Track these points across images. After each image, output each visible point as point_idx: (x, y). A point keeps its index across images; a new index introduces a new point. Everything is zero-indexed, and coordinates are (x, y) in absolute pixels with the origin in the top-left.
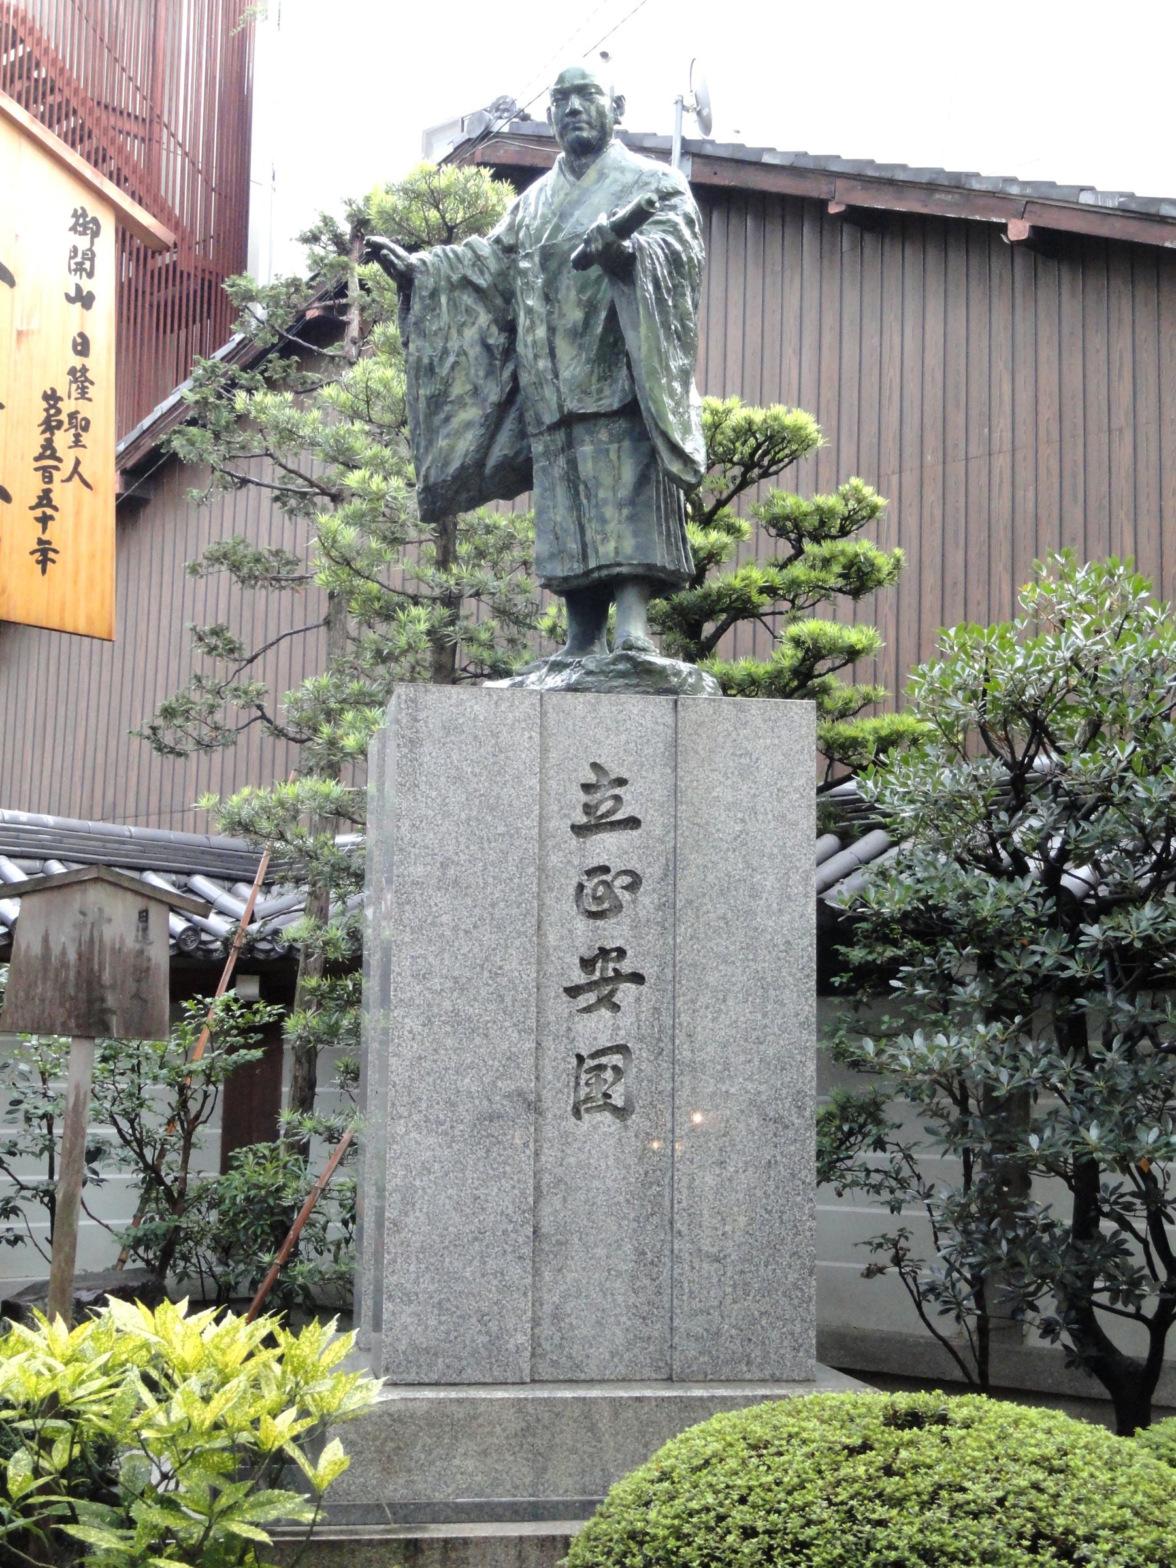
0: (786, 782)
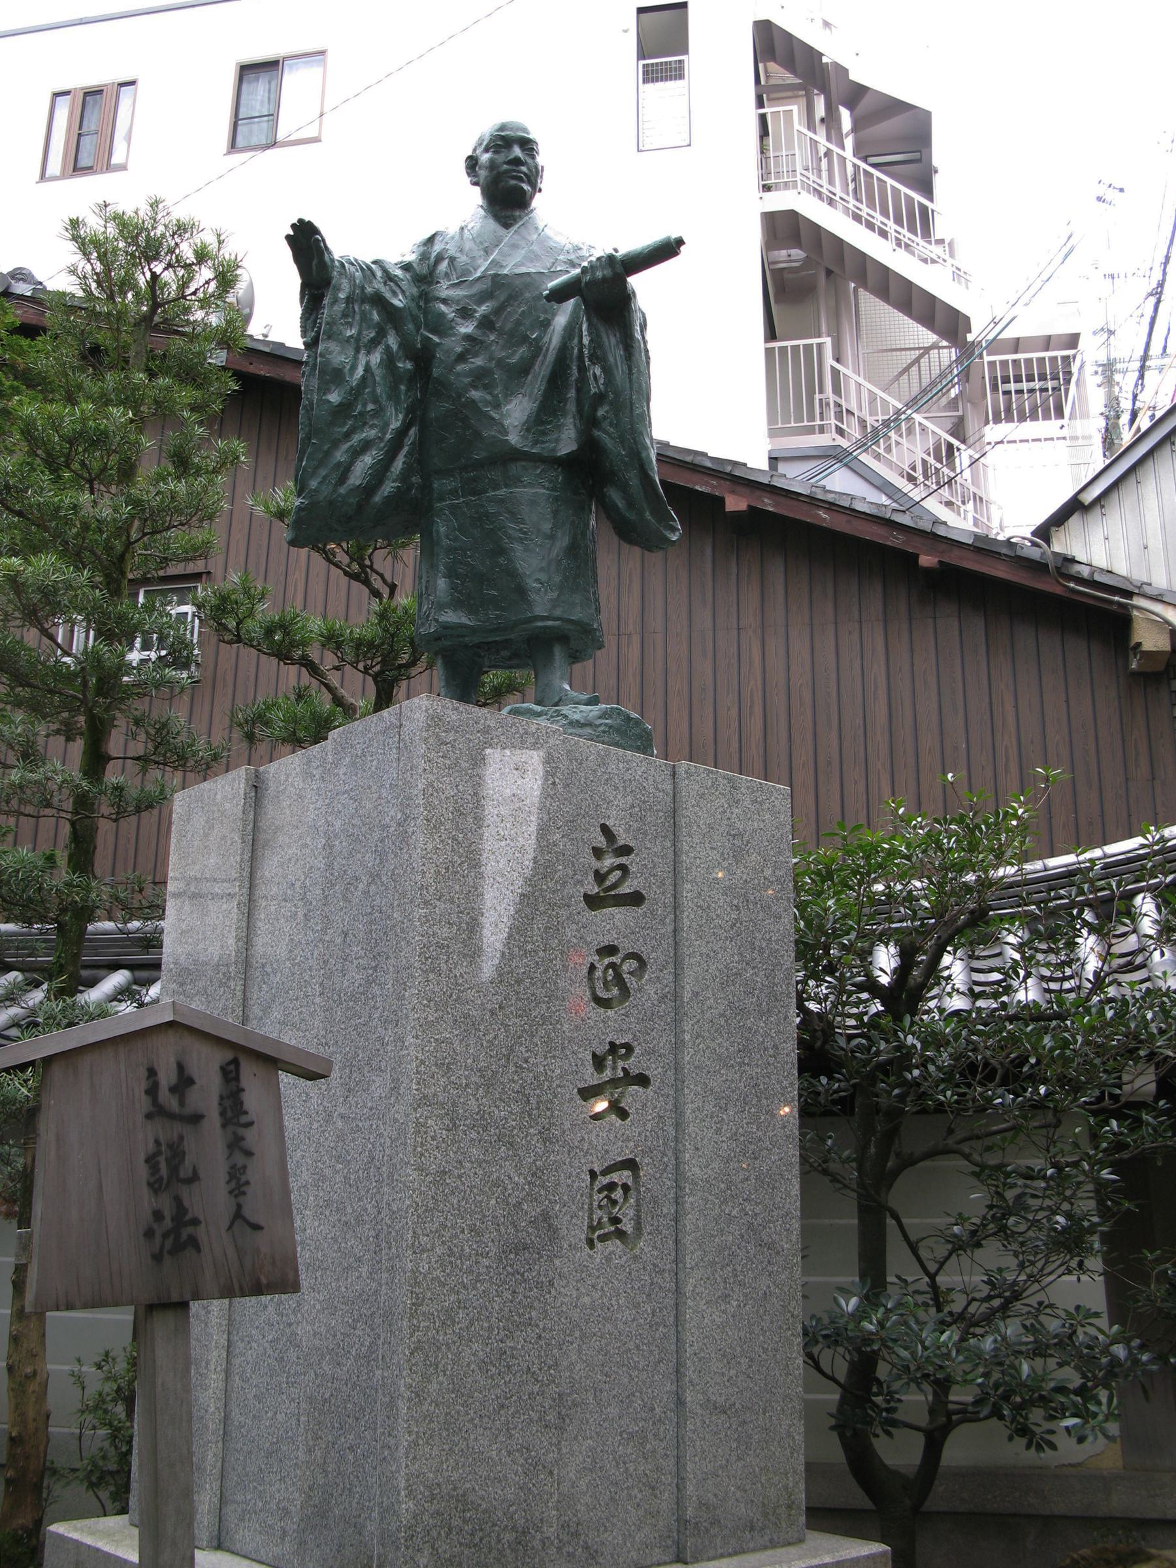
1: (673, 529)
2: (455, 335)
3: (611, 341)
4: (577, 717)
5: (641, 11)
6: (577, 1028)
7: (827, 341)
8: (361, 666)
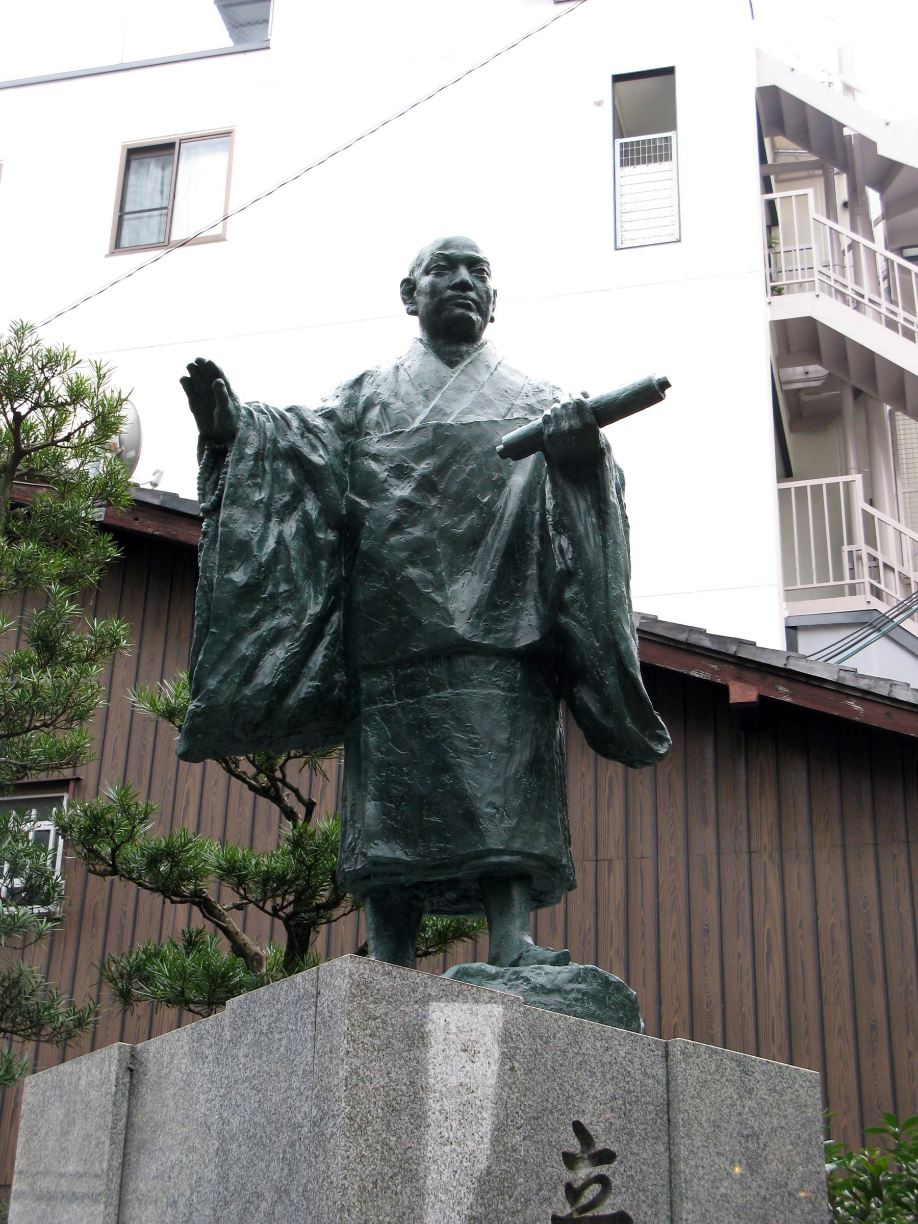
1: (661, 740)
2: (388, 499)
3: (580, 506)
4: (542, 980)
5: (617, 79)
7: (857, 479)
8: (269, 906)
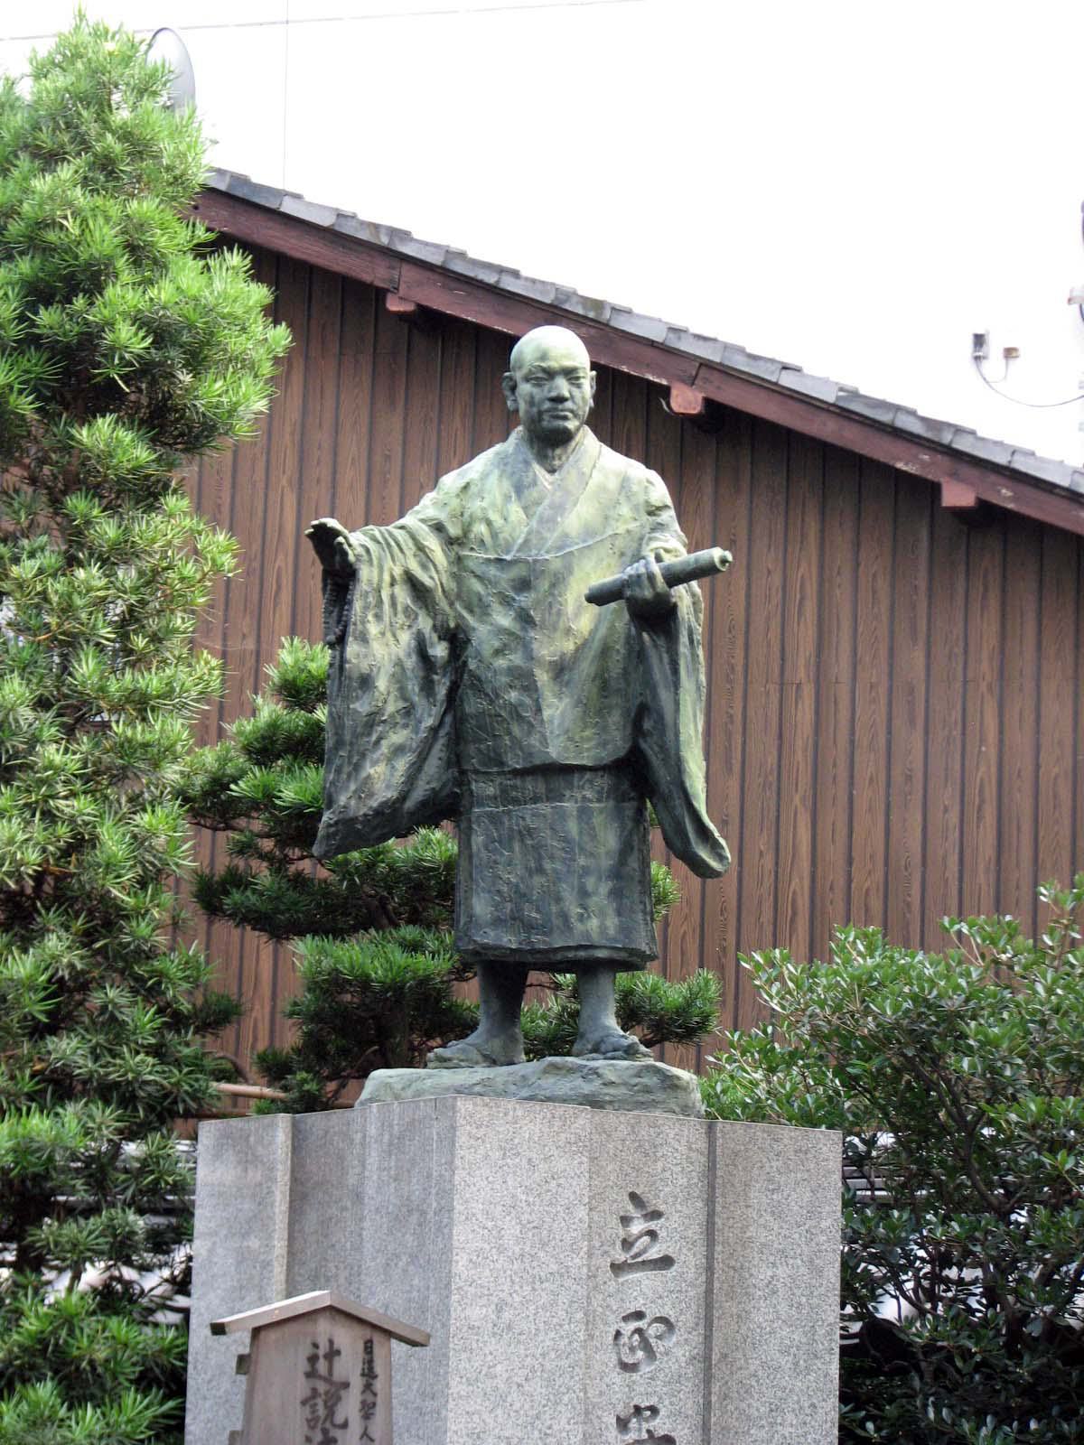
0: (813, 1223)
6: (601, 1394)
